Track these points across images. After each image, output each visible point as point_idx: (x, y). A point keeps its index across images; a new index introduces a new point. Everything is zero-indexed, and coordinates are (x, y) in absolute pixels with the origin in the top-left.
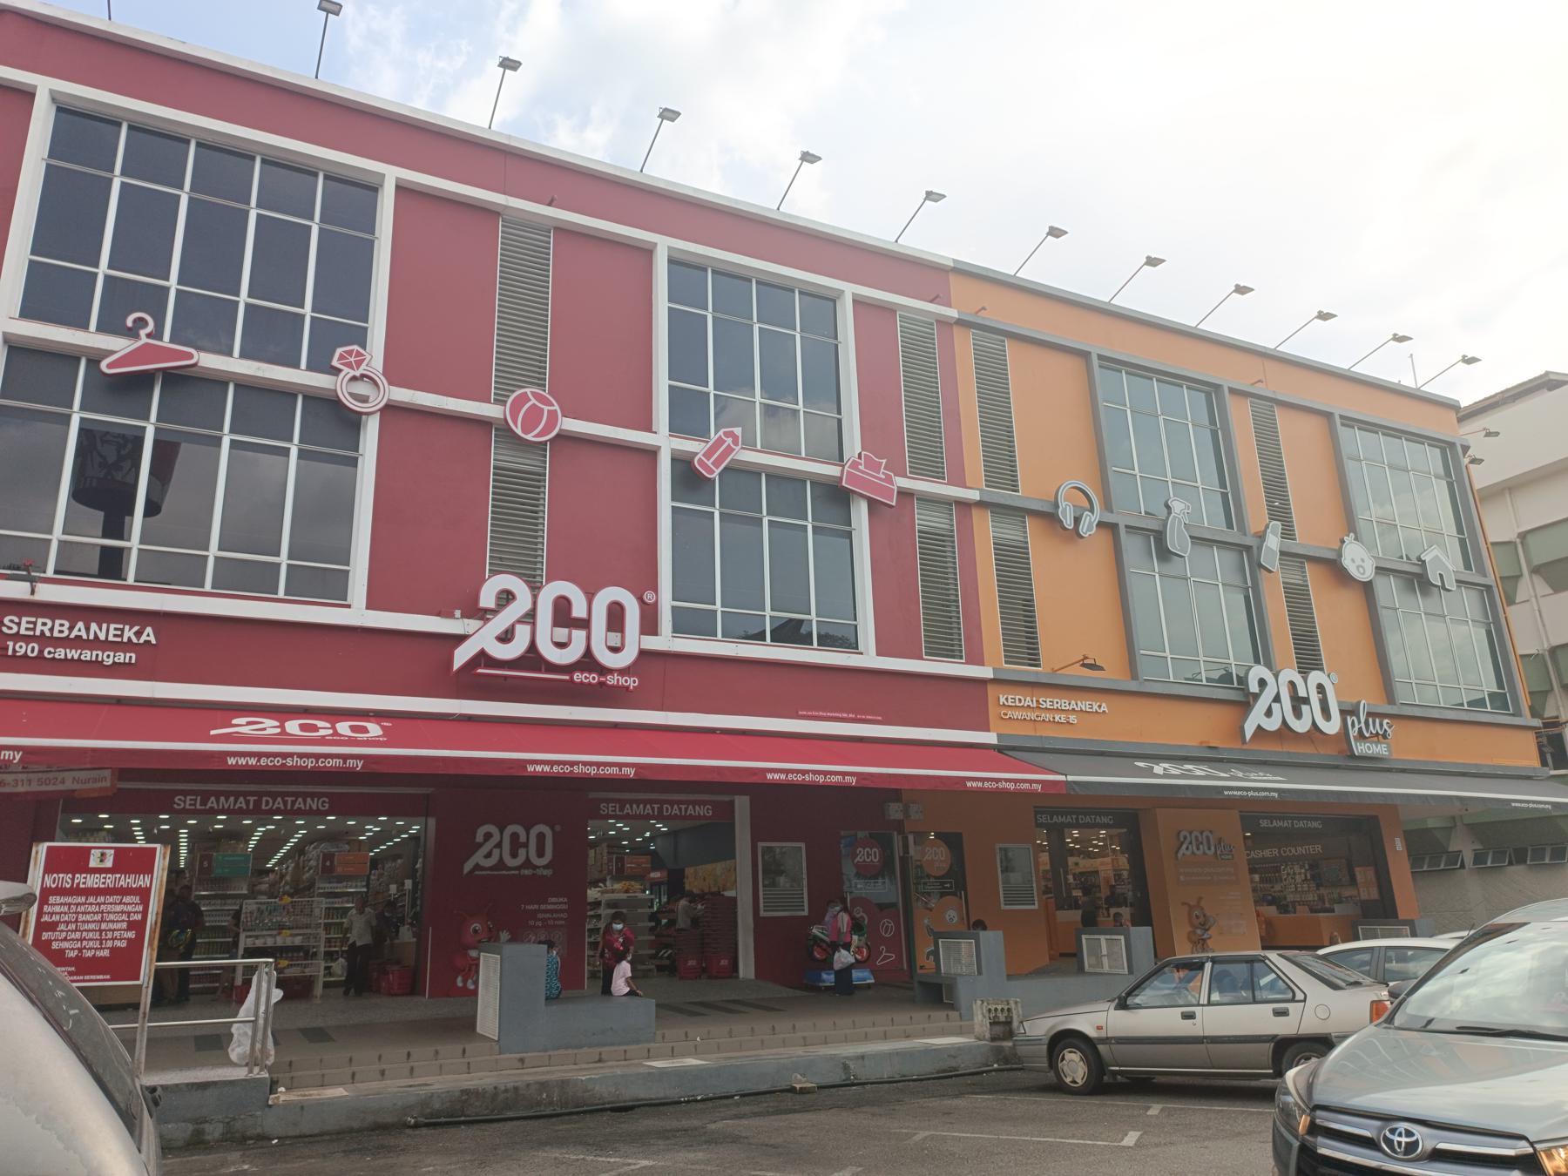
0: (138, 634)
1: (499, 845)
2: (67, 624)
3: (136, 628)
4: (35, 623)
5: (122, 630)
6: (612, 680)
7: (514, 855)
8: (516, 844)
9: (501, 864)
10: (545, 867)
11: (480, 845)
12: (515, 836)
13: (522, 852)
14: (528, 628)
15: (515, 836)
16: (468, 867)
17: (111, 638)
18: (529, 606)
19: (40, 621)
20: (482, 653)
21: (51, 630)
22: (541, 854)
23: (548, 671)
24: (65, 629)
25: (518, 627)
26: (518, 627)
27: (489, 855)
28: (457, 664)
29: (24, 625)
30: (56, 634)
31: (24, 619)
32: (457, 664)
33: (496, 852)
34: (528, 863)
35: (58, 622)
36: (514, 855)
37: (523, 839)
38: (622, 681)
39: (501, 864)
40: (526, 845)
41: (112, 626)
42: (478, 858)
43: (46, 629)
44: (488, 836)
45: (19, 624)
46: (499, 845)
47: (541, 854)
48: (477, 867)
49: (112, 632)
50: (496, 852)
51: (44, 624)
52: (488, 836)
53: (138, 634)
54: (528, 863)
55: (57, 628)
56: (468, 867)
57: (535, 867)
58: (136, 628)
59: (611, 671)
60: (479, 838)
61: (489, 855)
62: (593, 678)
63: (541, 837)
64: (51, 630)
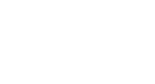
1: (56, 34)
7: (80, 48)
9: (59, 65)
10: (129, 70)
11: (27, 34)
13: (93, 45)
14: (55, 41)
18: (55, 25)
22: (123, 47)
25: (47, 40)
26: (47, 40)
27: (39, 50)
33: (52, 44)
34: (102, 65)
36: (80, 48)
37: (93, 24)
39: (59, 65)
40: (99, 34)
46: (56, 34)
47: (123, 47)
50: (52, 44)
54: (102, 65)
59: (120, 70)
61: (39, 50)
62: (106, 76)
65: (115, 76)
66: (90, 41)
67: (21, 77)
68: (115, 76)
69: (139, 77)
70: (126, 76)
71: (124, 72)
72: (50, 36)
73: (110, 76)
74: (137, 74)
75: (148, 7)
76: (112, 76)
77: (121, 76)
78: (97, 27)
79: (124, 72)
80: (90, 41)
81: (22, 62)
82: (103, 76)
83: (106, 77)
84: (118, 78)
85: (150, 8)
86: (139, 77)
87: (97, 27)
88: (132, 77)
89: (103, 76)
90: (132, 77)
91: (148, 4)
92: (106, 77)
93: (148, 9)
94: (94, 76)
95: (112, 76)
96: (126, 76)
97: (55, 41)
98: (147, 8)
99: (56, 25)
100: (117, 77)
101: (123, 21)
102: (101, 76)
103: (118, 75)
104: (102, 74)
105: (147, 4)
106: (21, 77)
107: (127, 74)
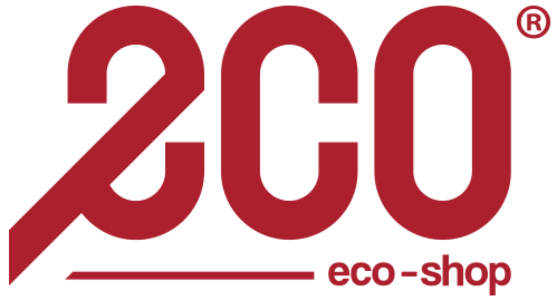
1: (201, 122)
6: (435, 274)
7: (289, 174)
8: (297, 125)
9: (213, 228)
10: (463, 250)
11: (95, 122)
12: (289, 72)
13: (336, 160)
14: (200, 147)
15: (289, 72)
16: (31, 237)
18: (198, 89)
20: (81, 226)
22: (443, 166)
25: (169, 145)
26: (169, 145)
27: (141, 179)
28: (18, 266)
32: (18, 266)
33: (185, 160)
34: (366, 227)
36: (289, 174)
37: (336, 87)
38: (465, 276)
39: (213, 228)
40: (355, 122)
42: (85, 192)
44: (135, 71)
46: (201, 122)
47: (443, 166)
48: (82, 242)
50: (185, 160)
52: (135, 71)
54: (366, 227)
56: (31, 237)
57: (416, 251)
59: (432, 250)
60: (86, 80)
61: (141, 179)
62: (381, 274)
63: (443, 80)
65: (414, 274)
68: (414, 274)
69: (500, 274)
70: (453, 273)
71: (445, 257)
72: (180, 130)
73: (398, 274)
74: (494, 266)
75: (533, 27)
76: (405, 274)
77: (435, 274)
78: (353, 99)
79: (445, 257)
80: (495, 295)
81: (81, 221)
82: (369, 274)
83: (384, 274)
84: (424, 282)
85: (538, 28)
87: (351, 96)
88: (477, 274)
89: (369, 274)
90: (477, 274)
91: (534, 15)
92: (384, 274)
93: (534, 31)
94: (341, 274)
95: (405, 274)
96: (453, 273)
97: (200, 147)
98: (529, 29)
99: (200, 89)
100: (421, 275)
101: (443, 80)
102: (362, 274)
103: (425, 267)
104: (365, 266)
105: (529, 16)
107: (458, 265)
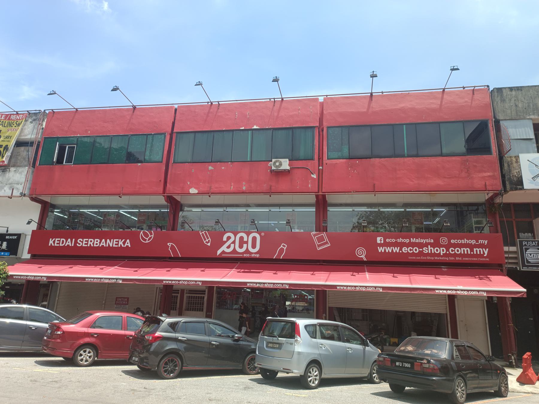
0: (124, 243)
1: (234, 242)
2: (99, 241)
3: (124, 240)
4: (88, 241)
5: (118, 242)
7: (241, 247)
8: (242, 242)
9: (234, 251)
10: (255, 253)
11: (225, 242)
12: (241, 238)
13: (245, 246)
15: (241, 238)
16: (219, 252)
17: (114, 246)
19: (90, 240)
21: (93, 244)
22: (254, 246)
23: (321, 293)
24: (98, 243)
27: (229, 247)
29: (84, 242)
30: (95, 245)
31: (85, 240)
33: (232, 245)
34: (247, 251)
35: (96, 240)
36: (241, 247)
37: (245, 239)
39: (234, 251)
40: (247, 242)
41: (115, 240)
42: (224, 248)
43: (91, 243)
44: (229, 238)
45: (82, 242)
46: (234, 242)
47: (254, 246)
48: (223, 252)
49: (115, 243)
51: (91, 241)
52: (229, 238)
53: (124, 243)
54: (247, 251)
55: (95, 243)
56: (219, 252)
58: (124, 240)
60: (225, 239)
61: (229, 247)
64: (93, 244)
66: (315, 208)
67: (16, 237)
69: (443, 250)
72: (232, 243)
83: (416, 250)
86: (443, 250)
106: (16, 237)
